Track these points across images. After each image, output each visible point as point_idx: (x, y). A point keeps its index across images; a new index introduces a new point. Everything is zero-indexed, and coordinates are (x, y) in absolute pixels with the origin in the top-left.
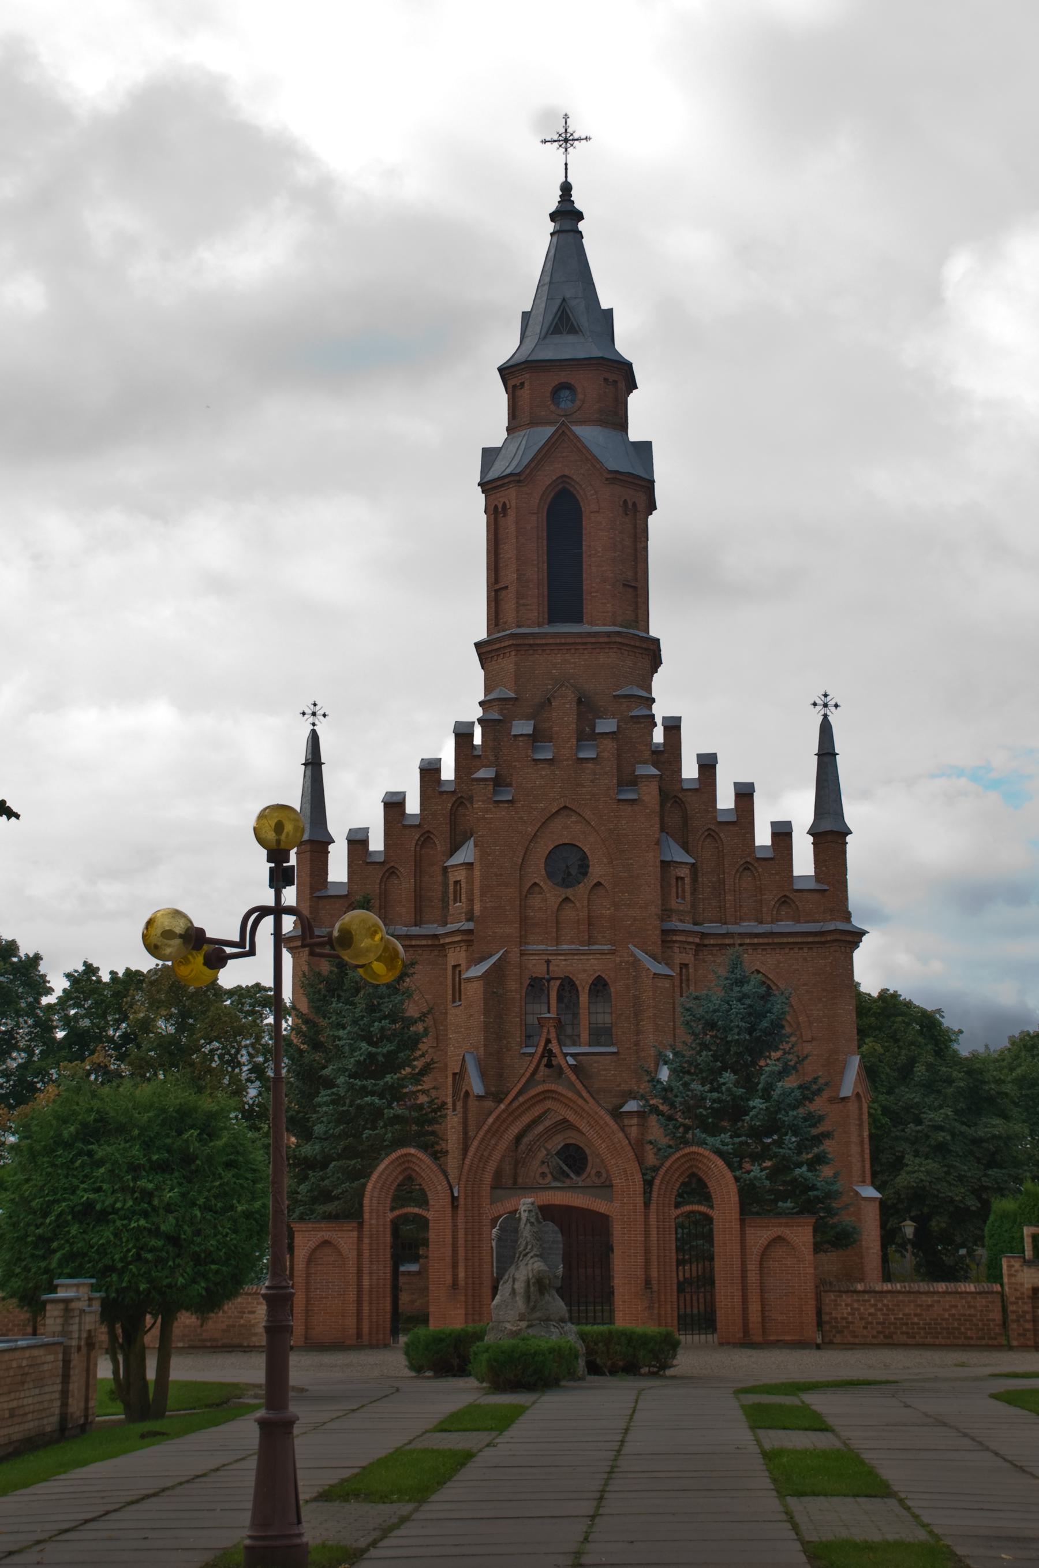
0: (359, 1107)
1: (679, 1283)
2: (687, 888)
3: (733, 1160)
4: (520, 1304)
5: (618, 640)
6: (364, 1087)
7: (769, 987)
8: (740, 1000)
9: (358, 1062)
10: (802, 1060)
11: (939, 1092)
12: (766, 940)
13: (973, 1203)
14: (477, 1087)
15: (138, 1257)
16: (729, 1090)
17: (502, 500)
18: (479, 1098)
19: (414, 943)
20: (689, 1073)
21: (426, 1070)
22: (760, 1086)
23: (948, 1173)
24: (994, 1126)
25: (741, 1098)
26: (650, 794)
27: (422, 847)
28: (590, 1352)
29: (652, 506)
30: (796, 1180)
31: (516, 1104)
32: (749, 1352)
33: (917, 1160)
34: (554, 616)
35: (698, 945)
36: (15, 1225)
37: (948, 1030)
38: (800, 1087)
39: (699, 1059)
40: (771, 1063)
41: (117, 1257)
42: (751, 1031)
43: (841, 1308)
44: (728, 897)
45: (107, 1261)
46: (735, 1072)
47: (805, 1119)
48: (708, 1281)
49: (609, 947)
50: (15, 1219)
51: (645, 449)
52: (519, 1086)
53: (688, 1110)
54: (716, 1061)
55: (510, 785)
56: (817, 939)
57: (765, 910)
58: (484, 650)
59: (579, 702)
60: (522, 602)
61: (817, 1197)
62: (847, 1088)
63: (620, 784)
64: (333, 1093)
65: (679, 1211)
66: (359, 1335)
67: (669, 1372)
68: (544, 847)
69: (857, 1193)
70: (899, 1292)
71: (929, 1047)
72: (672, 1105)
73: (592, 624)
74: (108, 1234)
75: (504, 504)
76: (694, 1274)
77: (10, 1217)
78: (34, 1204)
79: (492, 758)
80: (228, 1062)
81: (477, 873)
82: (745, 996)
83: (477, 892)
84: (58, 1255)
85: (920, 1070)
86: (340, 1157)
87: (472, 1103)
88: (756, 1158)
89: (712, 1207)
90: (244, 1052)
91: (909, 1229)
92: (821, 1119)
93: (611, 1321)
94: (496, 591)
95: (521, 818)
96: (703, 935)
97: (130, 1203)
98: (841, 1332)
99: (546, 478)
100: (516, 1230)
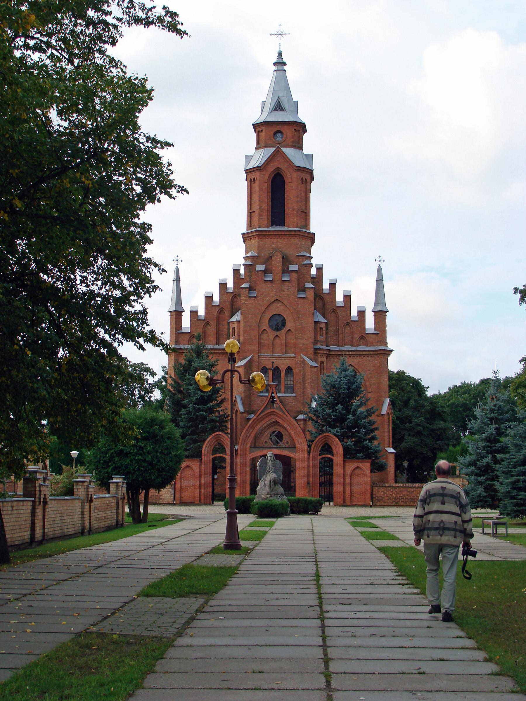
0: (197, 416)
1: (320, 484)
2: (324, 332)
3: (341, 437)
4: (267, 489)
5: (299, 233)
6: (199, 408)
7: (356, 372)
8: (344, 377)
9: (197, 399)
10: (367, 400)
11: (419, 411)
12: (354, 353)
13: (430, 454)
14: (241, 408)
15: (139, 469)
16: (340, 411)
17: (253, 177)
18: (242, 413)
19: (216, 352)
20: (324, 405)
21: (222, 401)
22: (352, 410)
23: (421, 443)
24: (440, 424)
25: (344, 415)
26: (310, 295)
27: (219, 314)
28: (291, 506)
29: (312, 179)
30: (364, 446)
31: (260, 416)
32: (346, 508)
33: (410, 438)
34: (274, 223)
35: (328, 354)
36: (95, 457)
37: (423, 386)
38: (367, 411)
39: (328, 400)
40: (356, 402)
41: (131, 469)
42: (348, 389)
43: (380, 492)
44: (340, 336)
45: (128, 470)
46: (342, 405)
47: (368, 423)
48: (331, 484)
49: (293, 355)
50: (95, 455)
51: (309, 157)
52: (261, 410)
53: (324, 419)
54: (335, 400)
55: (255, 290)
56: (374, 353)
57: (354, 341)
58: (245, 236)
59: (283, 258)
60: (261, 218)
61: (372, 452)
62: (384, 411)
63: (298, 291)
64: (187, 410)
65: (321, 457)
66: (200, 500)
67: (319, 513)
68: (268, 316)
69: (386, 450)
70: (402, 487)
71: (416, 393)
72: (318, 417)
73: (288, 227)
74: (128, 461)
75: (254, 178)
76: (323, 481)
77: (94, 454)
78: (102, 450)
79: (248, 280)
80: (130, 394)
81: (242, 325)
82: (347, 376)
83: (242, 332)
84: (111, 467)
85: (412, 403)
86: (190, 434)
87: (239, 415)
88: (349, 437)
89: (333, 455)
90: (136, 390)
91: (406, 464)
92: (374, 423)
93: (294, 495)
94: (251, 213)
95: (259, 304)
96: (330, 351)
97: (136, 451)
98: (379, 501)
99: (271, 168)
100: (266, 463)
